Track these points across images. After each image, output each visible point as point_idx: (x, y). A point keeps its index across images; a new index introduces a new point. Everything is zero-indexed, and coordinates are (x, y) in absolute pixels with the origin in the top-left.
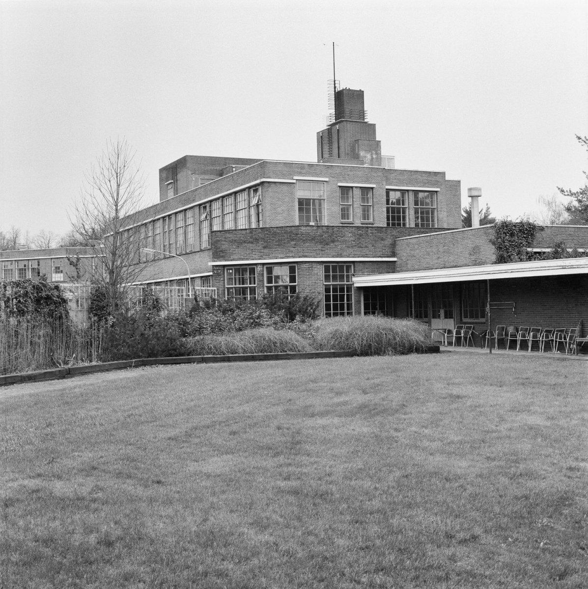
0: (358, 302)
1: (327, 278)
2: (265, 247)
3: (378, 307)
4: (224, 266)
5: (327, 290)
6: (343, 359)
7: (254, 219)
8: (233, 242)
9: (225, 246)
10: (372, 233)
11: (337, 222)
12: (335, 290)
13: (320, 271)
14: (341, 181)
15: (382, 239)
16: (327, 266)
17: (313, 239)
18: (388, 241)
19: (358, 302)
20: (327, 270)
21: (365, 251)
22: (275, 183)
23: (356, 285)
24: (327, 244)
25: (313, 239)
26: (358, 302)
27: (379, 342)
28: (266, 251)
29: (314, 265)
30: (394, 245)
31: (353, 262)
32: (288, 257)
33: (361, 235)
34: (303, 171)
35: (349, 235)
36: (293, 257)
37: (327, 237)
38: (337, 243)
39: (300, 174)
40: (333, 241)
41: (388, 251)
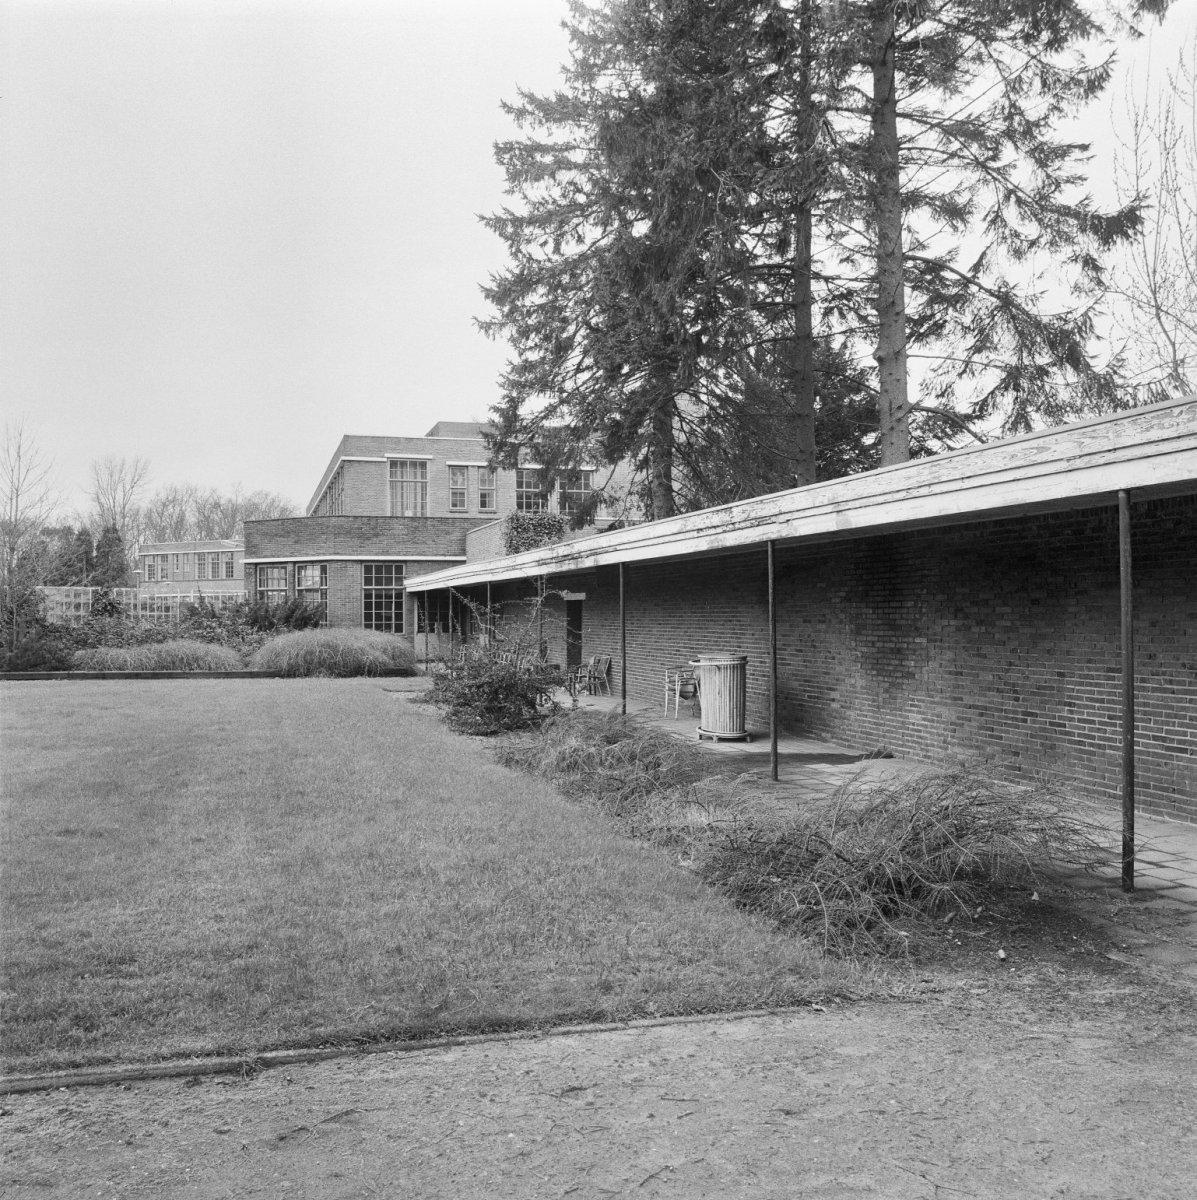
0: (411, 615)
1: (368, 581)
2: (296, 542)
3: (438, 617)
4: (256, 564)
5: (368, 596)
6: (262, 680)
7: (419, 509)
8: (265, 534)
9: (257, 540)
10: (434, 526)
11: (444, 512)
12: (378, 596)
13: (358, 573)
14: (450, 459)
15: (447, 533)
16: (368, 566)
17: (349, 532)
18: (456, 535)
19: (411, 611)
20: (368, 570)
21: (423, 547)
22: (359, 461)
23: (408, 590)
24: (368, 539)
25: (349, 532)
26: (411, 611)
27: (309, 663)
28: (298, 547)
29: (349, 565)
30: (463, 541)
31: (405, 562)
32: (319, 554)
33: (416, 528)
34: (401, 447)
35: (399, 528)
36: (324, 554)
37: (369, 528)
38: (381, 538)
39: (393, 450)
40: (377, 535)
41: (455, 548)
